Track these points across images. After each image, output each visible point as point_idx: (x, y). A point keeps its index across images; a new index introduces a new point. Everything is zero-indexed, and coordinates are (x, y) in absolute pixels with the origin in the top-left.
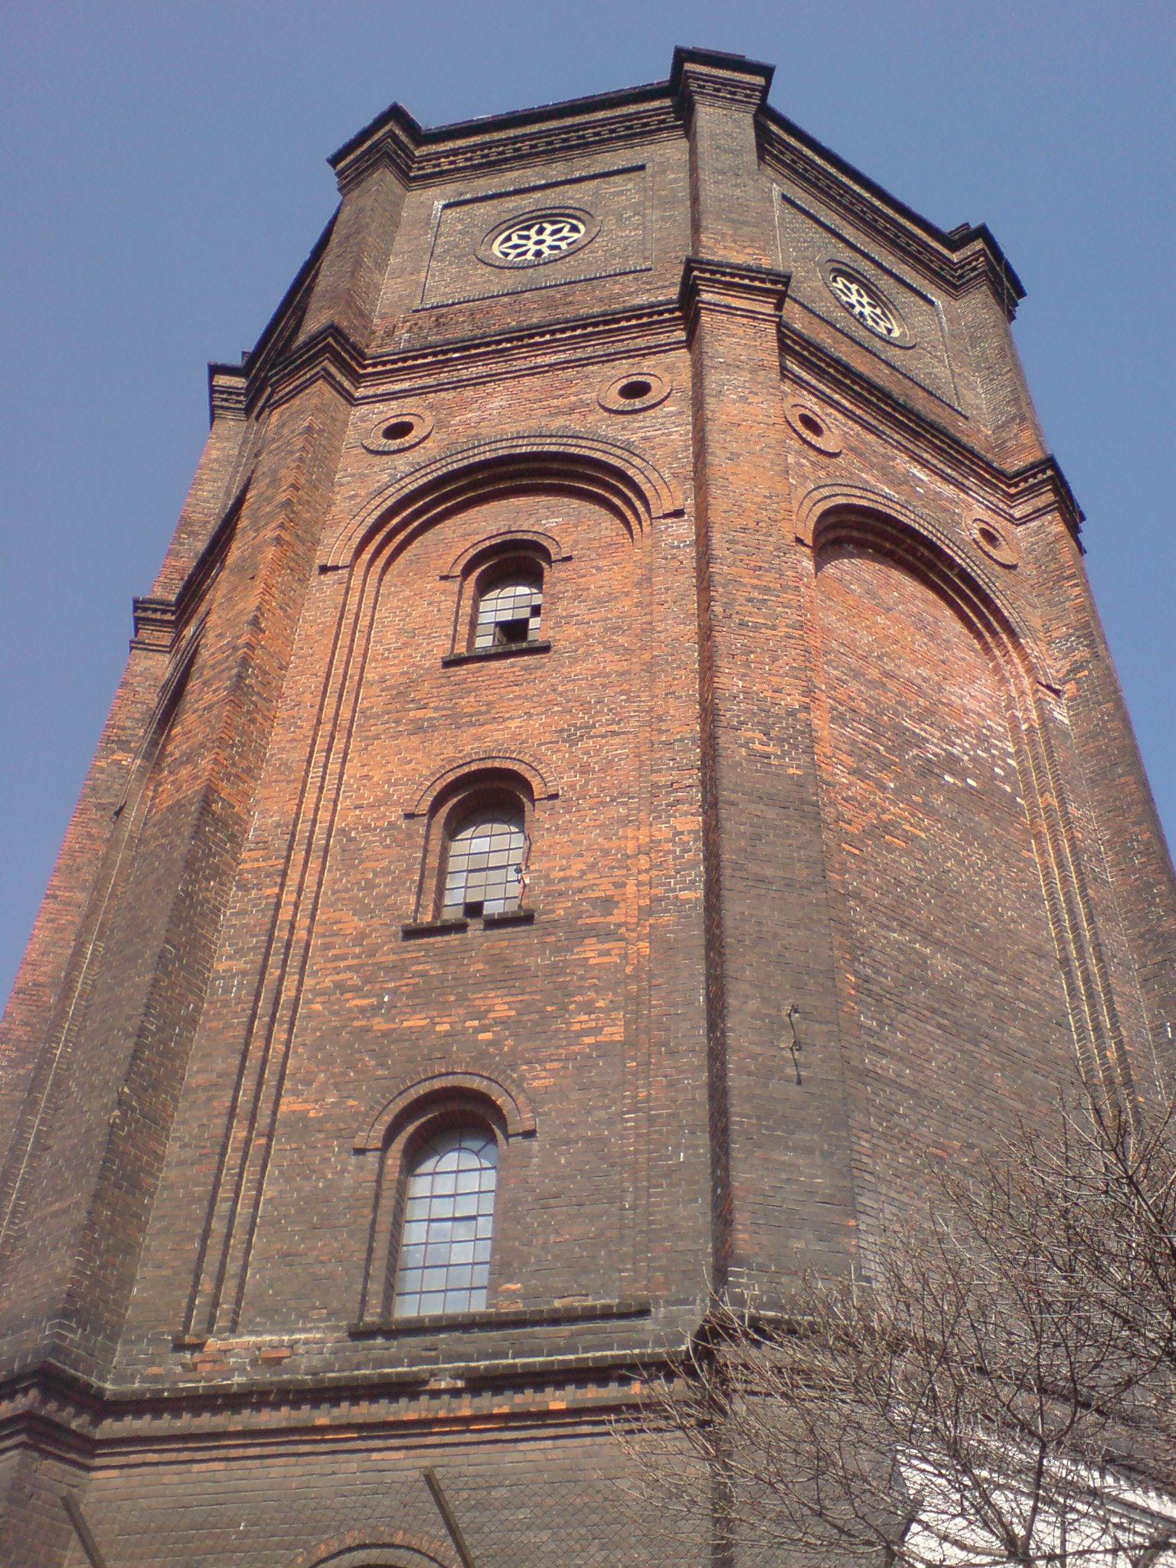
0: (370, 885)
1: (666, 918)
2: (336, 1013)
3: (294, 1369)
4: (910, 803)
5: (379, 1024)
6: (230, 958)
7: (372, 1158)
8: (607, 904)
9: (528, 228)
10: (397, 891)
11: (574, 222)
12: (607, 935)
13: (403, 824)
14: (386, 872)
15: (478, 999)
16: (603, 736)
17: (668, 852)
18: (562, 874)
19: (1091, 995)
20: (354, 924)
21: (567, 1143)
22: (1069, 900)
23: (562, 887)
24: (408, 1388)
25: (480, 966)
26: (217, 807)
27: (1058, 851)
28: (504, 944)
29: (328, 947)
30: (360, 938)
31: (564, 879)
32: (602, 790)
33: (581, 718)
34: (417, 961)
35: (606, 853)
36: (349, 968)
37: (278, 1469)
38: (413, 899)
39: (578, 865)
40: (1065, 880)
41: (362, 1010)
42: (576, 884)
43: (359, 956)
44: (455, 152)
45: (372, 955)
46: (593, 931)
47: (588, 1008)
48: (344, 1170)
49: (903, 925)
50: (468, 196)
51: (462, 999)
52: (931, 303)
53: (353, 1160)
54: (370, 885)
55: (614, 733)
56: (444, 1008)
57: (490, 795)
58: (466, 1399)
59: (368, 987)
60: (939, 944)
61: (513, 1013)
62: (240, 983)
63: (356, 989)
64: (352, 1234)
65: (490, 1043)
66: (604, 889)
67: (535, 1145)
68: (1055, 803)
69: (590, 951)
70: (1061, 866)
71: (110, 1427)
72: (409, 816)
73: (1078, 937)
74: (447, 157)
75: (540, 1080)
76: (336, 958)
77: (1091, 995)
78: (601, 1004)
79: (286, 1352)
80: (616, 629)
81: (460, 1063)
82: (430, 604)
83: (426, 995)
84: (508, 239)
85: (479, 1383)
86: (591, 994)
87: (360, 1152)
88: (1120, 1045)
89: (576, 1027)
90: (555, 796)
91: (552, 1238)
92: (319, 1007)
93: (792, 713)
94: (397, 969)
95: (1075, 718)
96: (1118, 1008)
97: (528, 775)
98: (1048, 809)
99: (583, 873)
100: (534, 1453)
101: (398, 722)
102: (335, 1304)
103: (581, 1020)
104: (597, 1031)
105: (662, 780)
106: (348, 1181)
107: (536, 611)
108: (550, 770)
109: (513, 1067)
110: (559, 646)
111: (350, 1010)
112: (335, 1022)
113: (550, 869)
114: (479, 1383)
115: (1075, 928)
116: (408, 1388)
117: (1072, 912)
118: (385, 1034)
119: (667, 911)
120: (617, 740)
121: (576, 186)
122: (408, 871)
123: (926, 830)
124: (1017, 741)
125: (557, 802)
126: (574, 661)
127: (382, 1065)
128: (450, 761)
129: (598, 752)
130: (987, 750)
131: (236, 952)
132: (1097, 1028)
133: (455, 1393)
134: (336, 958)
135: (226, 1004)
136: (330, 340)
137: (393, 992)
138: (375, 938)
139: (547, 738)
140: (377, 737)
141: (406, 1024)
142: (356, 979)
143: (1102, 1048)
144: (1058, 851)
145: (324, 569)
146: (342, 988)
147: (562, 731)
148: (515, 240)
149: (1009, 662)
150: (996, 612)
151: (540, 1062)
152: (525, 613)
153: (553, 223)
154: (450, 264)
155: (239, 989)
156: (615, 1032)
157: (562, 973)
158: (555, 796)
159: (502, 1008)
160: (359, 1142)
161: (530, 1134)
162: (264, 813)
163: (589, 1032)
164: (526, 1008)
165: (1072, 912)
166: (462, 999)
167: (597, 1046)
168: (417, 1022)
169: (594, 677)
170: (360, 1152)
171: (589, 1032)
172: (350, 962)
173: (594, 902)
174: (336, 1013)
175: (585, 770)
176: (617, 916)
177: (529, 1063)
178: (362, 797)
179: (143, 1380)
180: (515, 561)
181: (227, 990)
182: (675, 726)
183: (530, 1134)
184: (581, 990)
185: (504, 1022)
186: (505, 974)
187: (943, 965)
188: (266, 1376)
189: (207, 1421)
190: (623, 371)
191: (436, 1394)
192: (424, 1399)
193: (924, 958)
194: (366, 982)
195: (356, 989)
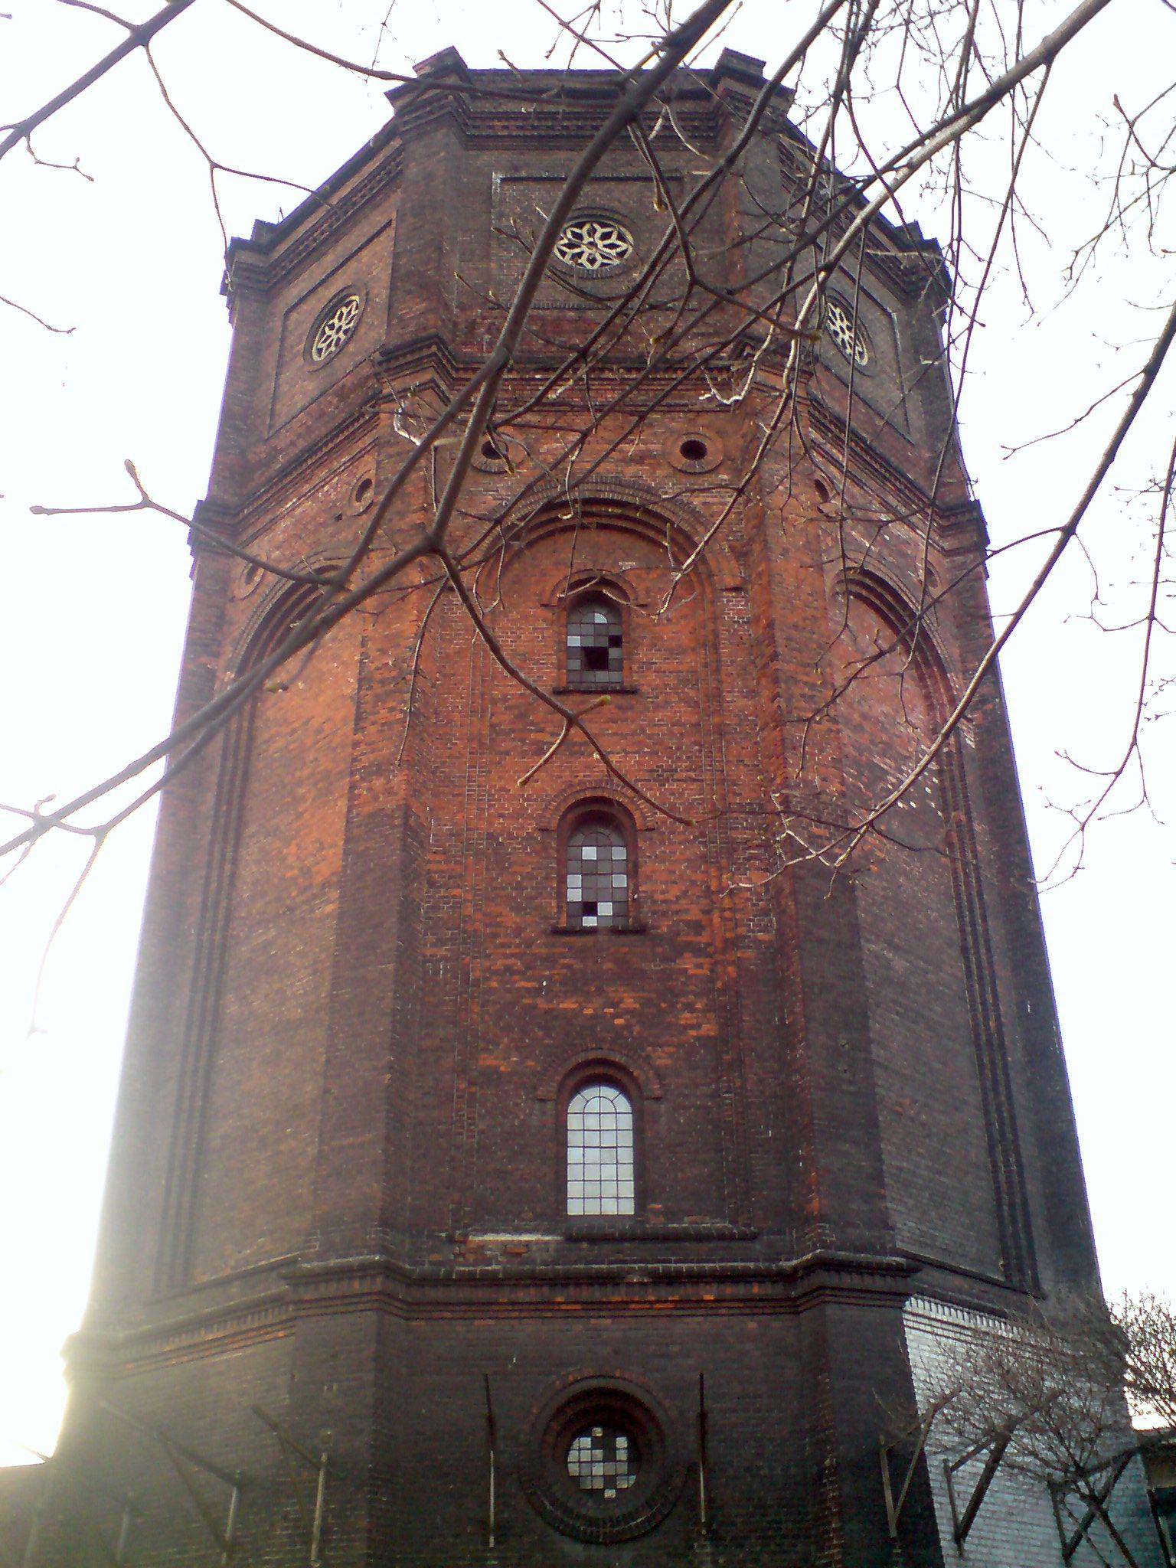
0: (519, 887)
1: (750, 953)
2: (509, 991)
3: (533, 1262)
5: (542, 1003)
6: (433, 945)
7: (549, 1106)
8: (697, 927)
9: (581, 226)
10: (540, 894)
11: (623, 230)
12: (698, 951)
14: (530, 877)
15: (612, 991)
17: (748, 899)
18: (662, 897)
19: (981, 978)
20: (512, 918)
21: (684, 1108)
22: (970, 902)
23: (664, 907)
29: (495, 935)
30: (518, 931)
31: (664, 901)
33: (665, 761)
35: (693, 883)
36: (512, 955)
38: (554, 903)
40: (968, 884)
41: (528, 990)
42: (675, 907)
43: (518, 946)
45: (530, 946)
46: (688, 946)
48: (531, 1114)
49: (878, 937)
50: (523, 174)
51: (600, 991)
52: (889, 315)
53: (537, 1106)
54: (519, 887)
55: (693, 780)
57: (596, 814)
60: (896, 949)
61: (637, 1006)
62: (445, 967)
65: (622, 1027)
67: (663, 1107)
68: (963, 818)
69: (687, 962)
72: (543, 830)
74: (499, 120)
76: (503, 945)
77: (981, 978)
78: (699, 1005)
79: (523, 1250)
80: (686, 682)
81: (603, 1040)
82: (535, 629)
83: (574, 984)
86: (692, 997)
88: (998, 1018)
91: (680, 1175)
92: (495, 984)
94: (550, 960)
95: (979, 743)
96: (999, 989)
98: (959, 823)
99: (678, 898)
101: (523, 740)
102: (538, 1210)
103: (686, 1017)
104: (697, 1026)
105: (741, 837)
106: (535, 1121)
107: (616, 641)
110: (645, 689)
111: (519, 989)
112: (509, 997)
115: (973, 924)
117: (971, 911)
118: (548, 1012)
119: (749, 947)
120: (694, 786)
121: (622, 186)
122: (547, 878)
125: (654, 835)
126: (657, 707)
127: (549, 1036)
129: (681, 794)
131: (438, 940)
132: (984, 1003)
133: (642, 1284)
134: (503, 945)
136: (434, 348)
137: (549, 979)
138: (530, 932)
139: (641, 775)
140: (508, 753)
142: (519, 965)
143: (986, 1019)
147: (651, 771)
149: (937, 690)
151: (661, 1046)
152: (604, 642)
153: (603, 225)
154: (515, 256)
155: (445, 973)
156: (709, 1029)
159: (629, 1002)
160: (541, 1092)
163: (692, 1027)
164: (647, 1003)
165: (971, 911)
166: (600, 991)
167: (698, 1038)
168: (569, 1005)
169: (673, 725)
170: (542, 1100)
171: (692, 1027)
172: (514, 950)
173: (687, 923)
174: (509, 991)
176: (704, 938)
178: (502, 807)
179: (431, 1263)
180: (592, 594)
181: (436, 972)
184: (685, 993)
186: (628, 975)
187: (900, 964)
188: (515, 1267)
189: (483, 1294)
191: (630, 1284)
193: (888, 960)
194: (529, 967)
195: (519, 972)
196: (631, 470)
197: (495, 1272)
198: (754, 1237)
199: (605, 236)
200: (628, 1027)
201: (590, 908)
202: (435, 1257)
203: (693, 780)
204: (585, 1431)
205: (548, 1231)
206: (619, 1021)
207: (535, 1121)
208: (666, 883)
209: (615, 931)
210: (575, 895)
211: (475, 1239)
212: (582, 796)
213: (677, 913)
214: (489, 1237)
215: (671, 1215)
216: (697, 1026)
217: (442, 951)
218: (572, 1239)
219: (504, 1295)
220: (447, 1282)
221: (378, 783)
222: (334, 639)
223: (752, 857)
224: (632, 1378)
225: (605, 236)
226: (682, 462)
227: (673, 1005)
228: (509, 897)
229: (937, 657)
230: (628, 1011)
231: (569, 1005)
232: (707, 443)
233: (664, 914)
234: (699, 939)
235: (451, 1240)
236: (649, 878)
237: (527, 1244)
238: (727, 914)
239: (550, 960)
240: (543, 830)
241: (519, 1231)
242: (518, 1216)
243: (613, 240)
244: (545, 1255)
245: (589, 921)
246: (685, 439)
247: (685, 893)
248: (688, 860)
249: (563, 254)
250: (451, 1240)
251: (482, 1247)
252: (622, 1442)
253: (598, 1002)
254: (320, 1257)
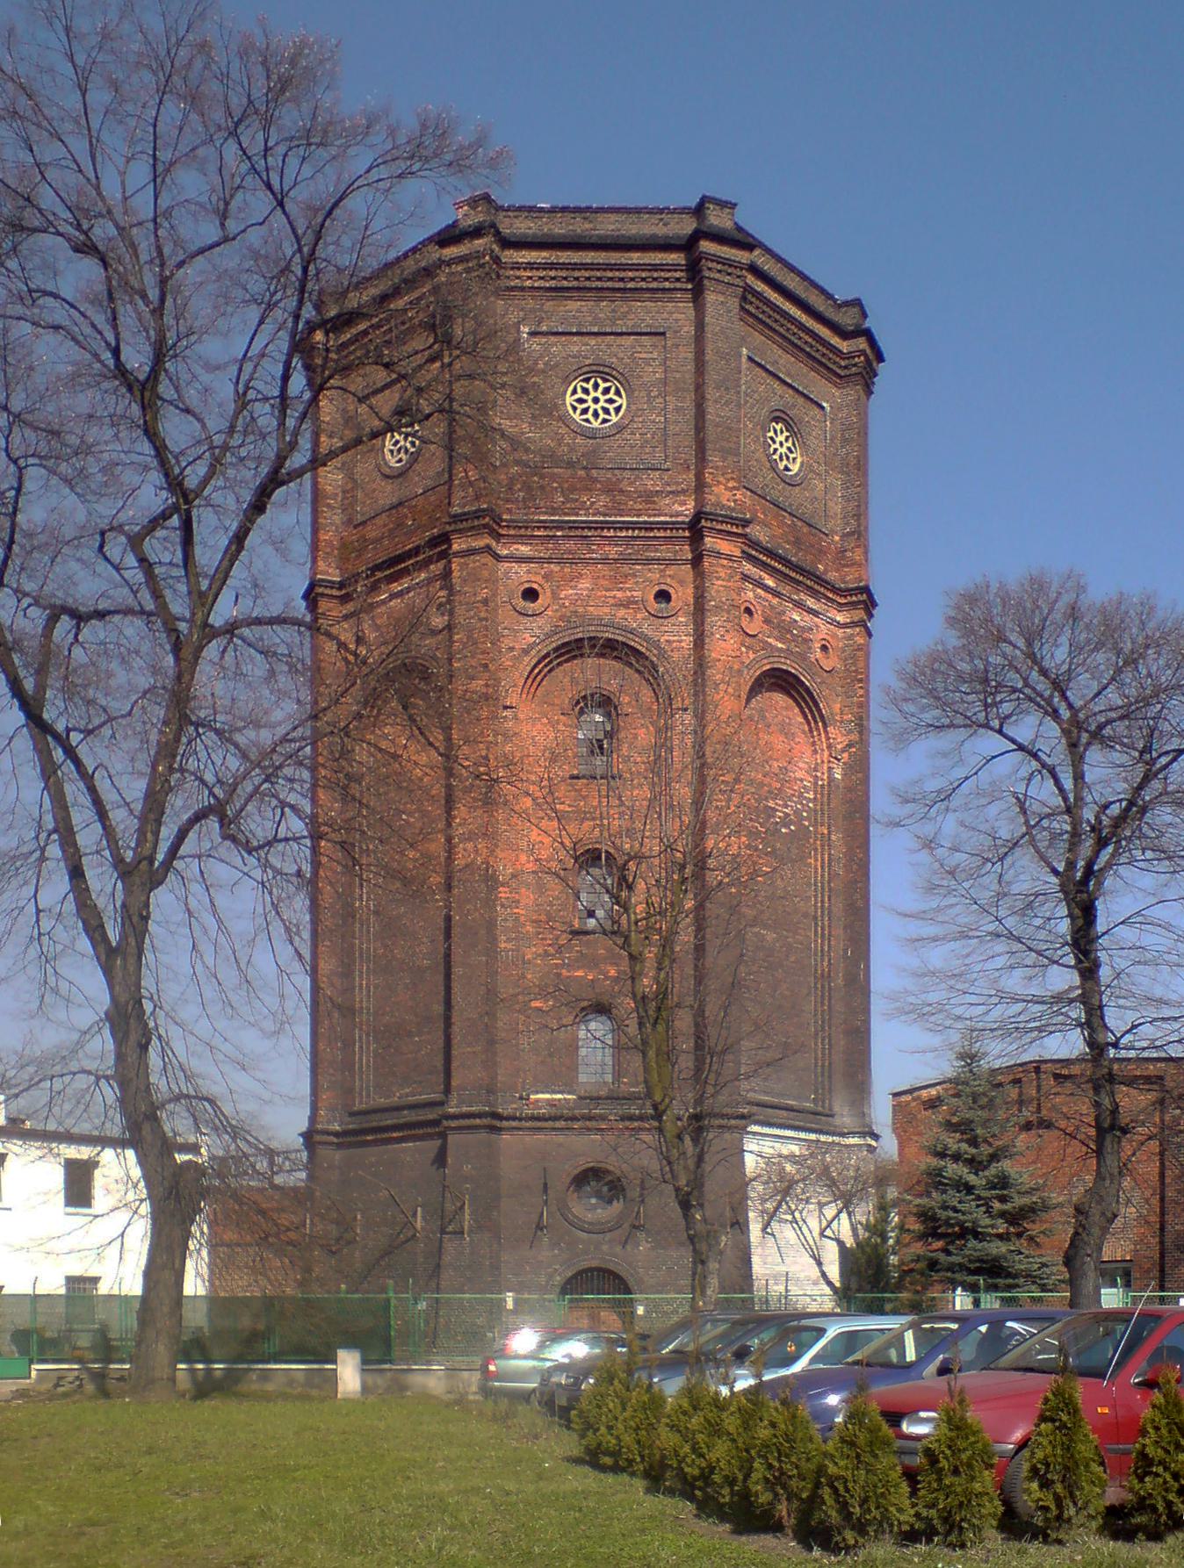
9: (587, 380)
37: (561, 1139)
44: (531, 266)
52: (823, 408)
71: (505, 1124)
84: (574, 392)
95: (844, 775)
116: (603, 1118)
145: (506, 708)
148: (580, 395)
150: (819, 710)
153: (605, 380)
159: (613, 973)
166: (596, 965)
168: (580, 973)
188: (553, 1111)
189: (539, 1124)
190: (653, 577)
196: (622, 612)
199: (607, 391)
201: (591, 914)
217: (509, 946)
218: (580, 1098)
219: (550, 1124)
221: (470, 845)
222: (220, 255)
224: (612, 1164)
225: (607, 391)
226: (654, 606)
229: (822, 716)
231: (580, 973)
232: (671, 591)
235: (521, 1098)
241: (554, 1092)
243: (611, 395)
245: (592, 923)
246: (657, 588)
249: (575, 409)
250: (521, 1098)
251: (537, 1101)
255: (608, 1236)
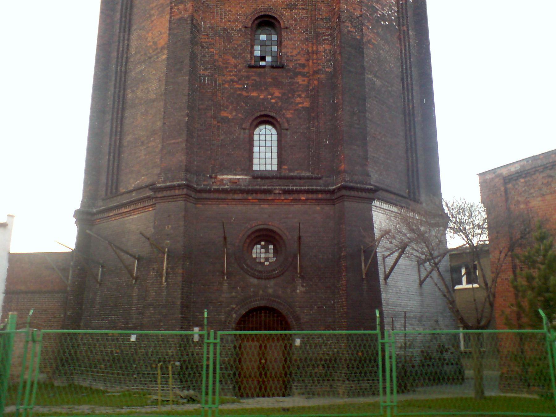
1: (323, 76)
4: (374, 33)
5: (244, 93)
7: (247, 131)
8: (303, 66)
13: (244, 30)
14: (241, 45)
15: (271, 90)
16: (300, 9)
20: (233, 61)
24: (269, 192)
25: (270, 80)
26: (195, 22)
27: (405, 45)
28: (276, 74)
29: (227, 68)
30: (235, 66)
31: (291, 56)
32: (300, 28)
34: (252, 76)
35: (303, 49)
36: (234, 75)
38: (249, 56)
39: (295, 53)
40: (406, 55)
41: (239, 89)
42: (295, 58)
43: (235, 72)
46: (300, 73)
47: (300, 96)
54: (236, 49)
56: (262, 91)
58: (282, 196)
59: (240, 82)
60: (377, 77)
63: (237, 82)
64: (245, 150)
66: (302, 61)
67: (288, 133)
70: (405, 50)
72: (245, 27)
73: (407, 72)
75: (289, 115)
83: (256, 86)
85: (286, 192)
86: (300, 93)
87: (245, 129)
89: (297, 101)
90: (287, 28)
93: (358, 17)
94: (248, 77)
97: (279, 19)
99: (296, 55)
100: (297, 207)
103: (298, 100)
104: (302, 103)
108: (286, 18)
109: (281, 110)
111: (236, 88)
113: (287, 52)
114: (286, 192)
115: (406, 69)
116: (269, 192)
118: (247, 97)
120: (304, 11)
122: (247, 46)
123: (377, 41)
124: (398, 8)
125: (288, 30)
127: (247, 106)
128: (256, 10)
130: (391, 11)
132: (408, 99)
133: (279, 194)
135: (205, 85)
137: (247, 84)
138: (240, 67)
141: (252, 95)
143: (409, 105)
144: (405, 45)
146: (232, 81)
156: (306, 104)
157: (293, 85)
158: (287, 28)
159: (277, 94)
160: (244, 126)
161: (287, 129)
162: (205, 22)
164: (284, 94)
166: (266, 89)
167: (302, 107)
168: (254, 94)
170: (245, 129)
173: (300, 64)
175: (295, 20)
176: (306, 70)
177: (285, 110)
181: (204, 80)
182: (324, 14)
183: (287, 129)
185: (278, 97)
186: (277, 84)
188: (234, 187)
189: (223, 196)
191: (275, 194)
192: (273, 195)
193: (374, 82)
197: (227, 189)
198: (320, 178)
200: (276, 103)
202: (205, 183)
203: (303, 9)
204: (259, 243)
205: (246, 175)
206: (273, 101)
207: (242, 136)
208: (292, 49)
209: (272, 67)
210: (257, 53)
211: (220, 177)
212: (261, 14)
213: (296, 60)
214: (225, 177)
215: (290, 170)
216: (302, 103)
217: (207, 73)
220: (209, 191)
223: (325, 39)
224: (274, 225)
227: (293, 96)
228: (232, 53)
230: (276, 97)
231: (254, 94)
233: (291, 61)
234: (304, 71)
236: (286, 47)
237: (239, 179)
238: (315, 61)
239: (248, 77)
240: (245, 27)
241: (236, 175)
242: (235, 170)
244: (245, 183)
247: (299, 53)
248: (301, 40)
252: (271, 247)
253: (265, 93)
254: (164, 182)
255: (272, 282)
